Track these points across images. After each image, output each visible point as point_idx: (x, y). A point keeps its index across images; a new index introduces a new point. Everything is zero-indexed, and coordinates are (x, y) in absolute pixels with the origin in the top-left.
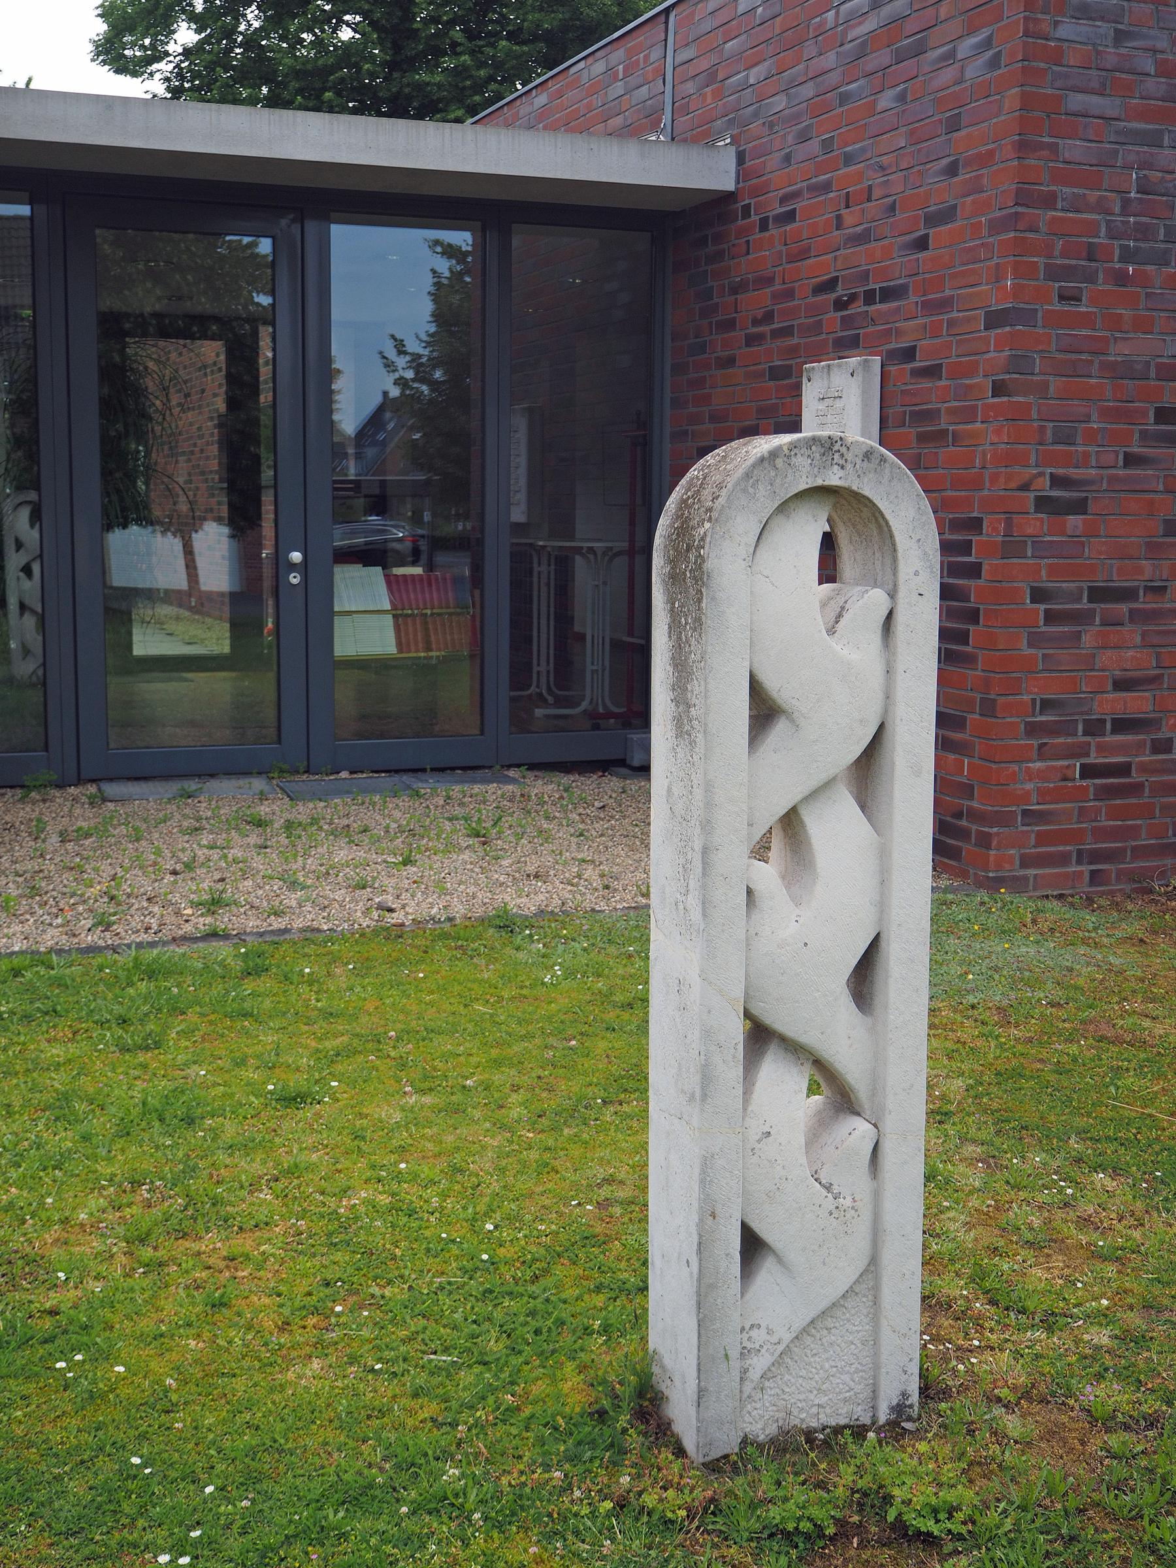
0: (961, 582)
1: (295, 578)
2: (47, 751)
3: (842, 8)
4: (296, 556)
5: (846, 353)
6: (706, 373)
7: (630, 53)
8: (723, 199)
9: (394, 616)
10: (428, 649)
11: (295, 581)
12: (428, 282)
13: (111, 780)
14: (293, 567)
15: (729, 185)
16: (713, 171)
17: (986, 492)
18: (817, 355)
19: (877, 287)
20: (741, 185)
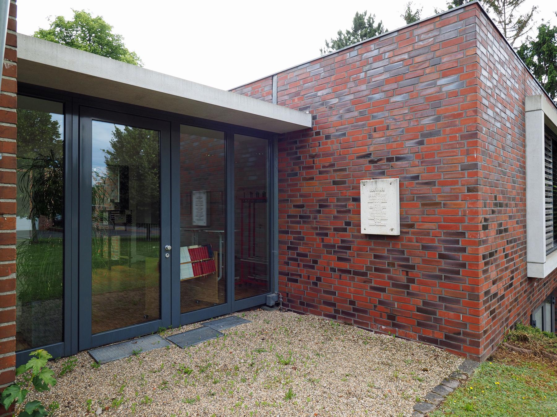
0: (447, 253)
1: (167, 255)
2: (63, 340)
3: (368, 72)
4: (169, 247)
5: (377, 177)
6: (298, 182)
7: (253, 89)
8: (308, 129)
9: (192, 263)
10: (202, 274)
11: (167, 256)
12: (104, 160)
13: (95, 348)
14: (167, 251)
15: (309, 125)
16: (304, 120)
17: (466, 224)
18: (364, 177)
19: (394, 156)
20: (314, 125)
